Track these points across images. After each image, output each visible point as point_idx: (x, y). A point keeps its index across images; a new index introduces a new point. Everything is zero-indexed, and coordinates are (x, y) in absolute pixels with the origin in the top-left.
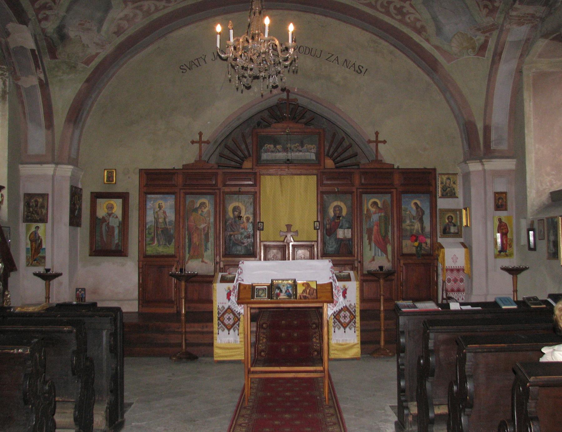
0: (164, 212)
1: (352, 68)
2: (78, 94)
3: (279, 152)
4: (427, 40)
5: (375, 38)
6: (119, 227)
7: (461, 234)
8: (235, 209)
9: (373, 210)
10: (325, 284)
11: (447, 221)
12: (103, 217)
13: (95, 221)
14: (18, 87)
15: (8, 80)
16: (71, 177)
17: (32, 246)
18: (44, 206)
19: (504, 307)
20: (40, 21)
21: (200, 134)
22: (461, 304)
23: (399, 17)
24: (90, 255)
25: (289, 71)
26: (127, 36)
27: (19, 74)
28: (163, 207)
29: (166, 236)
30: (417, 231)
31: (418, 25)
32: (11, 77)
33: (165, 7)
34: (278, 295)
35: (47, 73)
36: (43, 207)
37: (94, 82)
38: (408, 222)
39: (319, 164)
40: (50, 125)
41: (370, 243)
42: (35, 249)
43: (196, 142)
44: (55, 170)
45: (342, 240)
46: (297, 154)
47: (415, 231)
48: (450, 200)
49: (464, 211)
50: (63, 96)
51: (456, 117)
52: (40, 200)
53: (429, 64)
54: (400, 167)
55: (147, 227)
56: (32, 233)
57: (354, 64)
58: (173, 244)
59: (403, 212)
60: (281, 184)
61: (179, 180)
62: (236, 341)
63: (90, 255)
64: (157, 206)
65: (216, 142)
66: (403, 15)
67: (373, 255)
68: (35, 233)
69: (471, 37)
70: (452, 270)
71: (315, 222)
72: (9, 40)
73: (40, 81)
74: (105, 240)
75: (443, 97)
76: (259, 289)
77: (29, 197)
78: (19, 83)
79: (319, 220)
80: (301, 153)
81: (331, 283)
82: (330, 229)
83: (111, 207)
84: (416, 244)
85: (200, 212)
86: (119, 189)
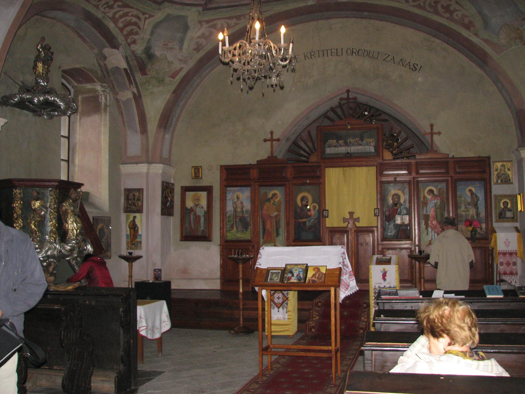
0: (242, 203)
1: (408, 66)
2: (168, 103)
3: (341, 146)
4: (476, 35)
5: (427, 36)
6: (204, 216)
7: (517, 219)
8: (303, 199)
9: (429, 197)
10: (334, 269)
11: (502, 207)
12: (191, 208)
13: (185, 212)
14: (117, 100)
15: (108, 95)
16: (162, 174)
17: (130, 232)
18: (140, 199)
19: (488, 296)
20: (129, 45)
21: (272, 133)
22: (446, 292)
23: (448, 15)
24: (181, 240)
25: (288, 71)
26: (205, 52)
27: (117, 90)
28: (241, 198)
29: (245, 224)
30: (472, 216)
31: (466, 21)
32: (111, 93)
33: (236, 24)
34: (289, 279)
35: (139, 86)
36: (139, 200)
37: (178, 93)
38: (463, 208)
39: (378, 155)
40: (144, 130)
41: (427, 228)
42: (133, 235)
43: (268, 140)
44: (148, 169)
45: (400, 226)
46: (357, 147)
47: (470, 217)
48: (506, 186)
49: (519, 197)
50: (155, 105)
51: (509, 107)
52: (137, 194)
53: (480, 58)
54: (455, 156)
55: (227, 216)
56: (131, 222)
57: (409, 62)
58: (249, 230)
59: (458, 199)
60: (344, 175)
61: (254, 174)
62: (284, 318)
63: (181, 240)
64: (236, 197)
65: (288, 140)
66: (451, 13)
67: (430, 239)
68: (134, 221)
69: (518, 28)
70: (504, 254)
71: (375, 209)
72: (106, 62)
73: (134, 94)
74: (193, 226)
75: (495, 87)
76: (273, 273)
77: (128, 191)
78: (118, 97)
79: (379, 207)
80: (361, 147)
81: (340, 268)
82: (389, 215)
83: (197, 199)
84: (470, 228)
85: (272, 202)
86: (204, 182)
